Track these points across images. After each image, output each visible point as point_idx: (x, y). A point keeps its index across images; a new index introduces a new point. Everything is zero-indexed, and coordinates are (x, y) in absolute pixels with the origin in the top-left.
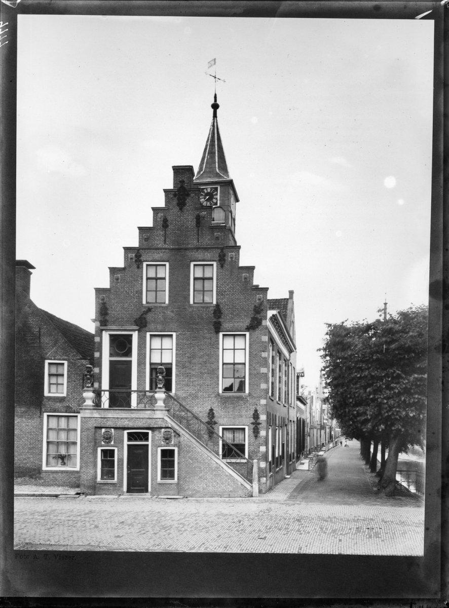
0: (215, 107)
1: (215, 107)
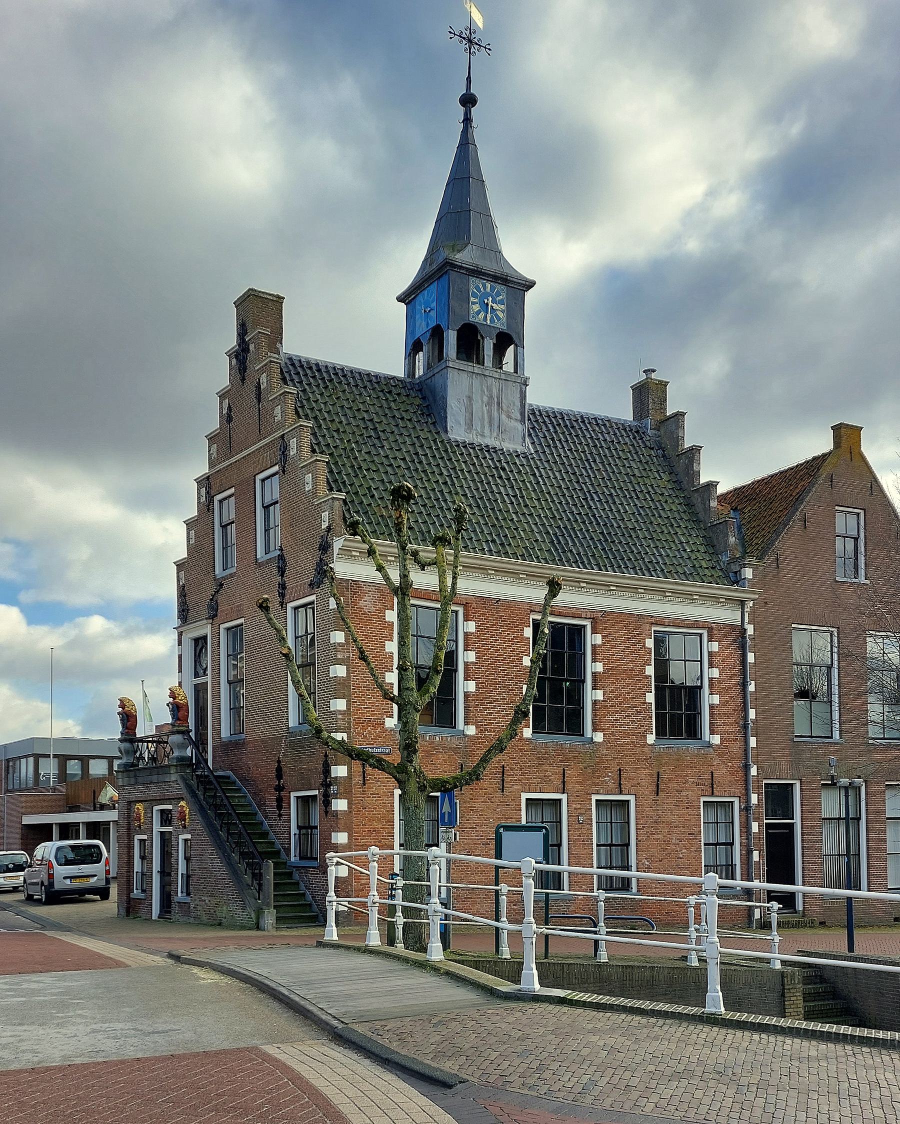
0: (468, 101)
1: (468, 101)
